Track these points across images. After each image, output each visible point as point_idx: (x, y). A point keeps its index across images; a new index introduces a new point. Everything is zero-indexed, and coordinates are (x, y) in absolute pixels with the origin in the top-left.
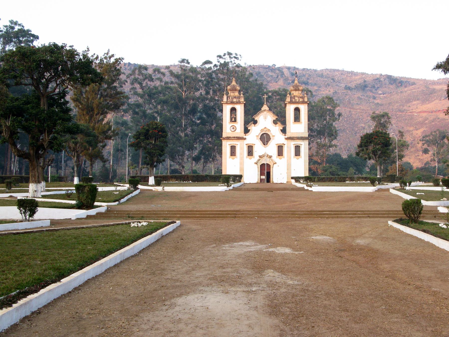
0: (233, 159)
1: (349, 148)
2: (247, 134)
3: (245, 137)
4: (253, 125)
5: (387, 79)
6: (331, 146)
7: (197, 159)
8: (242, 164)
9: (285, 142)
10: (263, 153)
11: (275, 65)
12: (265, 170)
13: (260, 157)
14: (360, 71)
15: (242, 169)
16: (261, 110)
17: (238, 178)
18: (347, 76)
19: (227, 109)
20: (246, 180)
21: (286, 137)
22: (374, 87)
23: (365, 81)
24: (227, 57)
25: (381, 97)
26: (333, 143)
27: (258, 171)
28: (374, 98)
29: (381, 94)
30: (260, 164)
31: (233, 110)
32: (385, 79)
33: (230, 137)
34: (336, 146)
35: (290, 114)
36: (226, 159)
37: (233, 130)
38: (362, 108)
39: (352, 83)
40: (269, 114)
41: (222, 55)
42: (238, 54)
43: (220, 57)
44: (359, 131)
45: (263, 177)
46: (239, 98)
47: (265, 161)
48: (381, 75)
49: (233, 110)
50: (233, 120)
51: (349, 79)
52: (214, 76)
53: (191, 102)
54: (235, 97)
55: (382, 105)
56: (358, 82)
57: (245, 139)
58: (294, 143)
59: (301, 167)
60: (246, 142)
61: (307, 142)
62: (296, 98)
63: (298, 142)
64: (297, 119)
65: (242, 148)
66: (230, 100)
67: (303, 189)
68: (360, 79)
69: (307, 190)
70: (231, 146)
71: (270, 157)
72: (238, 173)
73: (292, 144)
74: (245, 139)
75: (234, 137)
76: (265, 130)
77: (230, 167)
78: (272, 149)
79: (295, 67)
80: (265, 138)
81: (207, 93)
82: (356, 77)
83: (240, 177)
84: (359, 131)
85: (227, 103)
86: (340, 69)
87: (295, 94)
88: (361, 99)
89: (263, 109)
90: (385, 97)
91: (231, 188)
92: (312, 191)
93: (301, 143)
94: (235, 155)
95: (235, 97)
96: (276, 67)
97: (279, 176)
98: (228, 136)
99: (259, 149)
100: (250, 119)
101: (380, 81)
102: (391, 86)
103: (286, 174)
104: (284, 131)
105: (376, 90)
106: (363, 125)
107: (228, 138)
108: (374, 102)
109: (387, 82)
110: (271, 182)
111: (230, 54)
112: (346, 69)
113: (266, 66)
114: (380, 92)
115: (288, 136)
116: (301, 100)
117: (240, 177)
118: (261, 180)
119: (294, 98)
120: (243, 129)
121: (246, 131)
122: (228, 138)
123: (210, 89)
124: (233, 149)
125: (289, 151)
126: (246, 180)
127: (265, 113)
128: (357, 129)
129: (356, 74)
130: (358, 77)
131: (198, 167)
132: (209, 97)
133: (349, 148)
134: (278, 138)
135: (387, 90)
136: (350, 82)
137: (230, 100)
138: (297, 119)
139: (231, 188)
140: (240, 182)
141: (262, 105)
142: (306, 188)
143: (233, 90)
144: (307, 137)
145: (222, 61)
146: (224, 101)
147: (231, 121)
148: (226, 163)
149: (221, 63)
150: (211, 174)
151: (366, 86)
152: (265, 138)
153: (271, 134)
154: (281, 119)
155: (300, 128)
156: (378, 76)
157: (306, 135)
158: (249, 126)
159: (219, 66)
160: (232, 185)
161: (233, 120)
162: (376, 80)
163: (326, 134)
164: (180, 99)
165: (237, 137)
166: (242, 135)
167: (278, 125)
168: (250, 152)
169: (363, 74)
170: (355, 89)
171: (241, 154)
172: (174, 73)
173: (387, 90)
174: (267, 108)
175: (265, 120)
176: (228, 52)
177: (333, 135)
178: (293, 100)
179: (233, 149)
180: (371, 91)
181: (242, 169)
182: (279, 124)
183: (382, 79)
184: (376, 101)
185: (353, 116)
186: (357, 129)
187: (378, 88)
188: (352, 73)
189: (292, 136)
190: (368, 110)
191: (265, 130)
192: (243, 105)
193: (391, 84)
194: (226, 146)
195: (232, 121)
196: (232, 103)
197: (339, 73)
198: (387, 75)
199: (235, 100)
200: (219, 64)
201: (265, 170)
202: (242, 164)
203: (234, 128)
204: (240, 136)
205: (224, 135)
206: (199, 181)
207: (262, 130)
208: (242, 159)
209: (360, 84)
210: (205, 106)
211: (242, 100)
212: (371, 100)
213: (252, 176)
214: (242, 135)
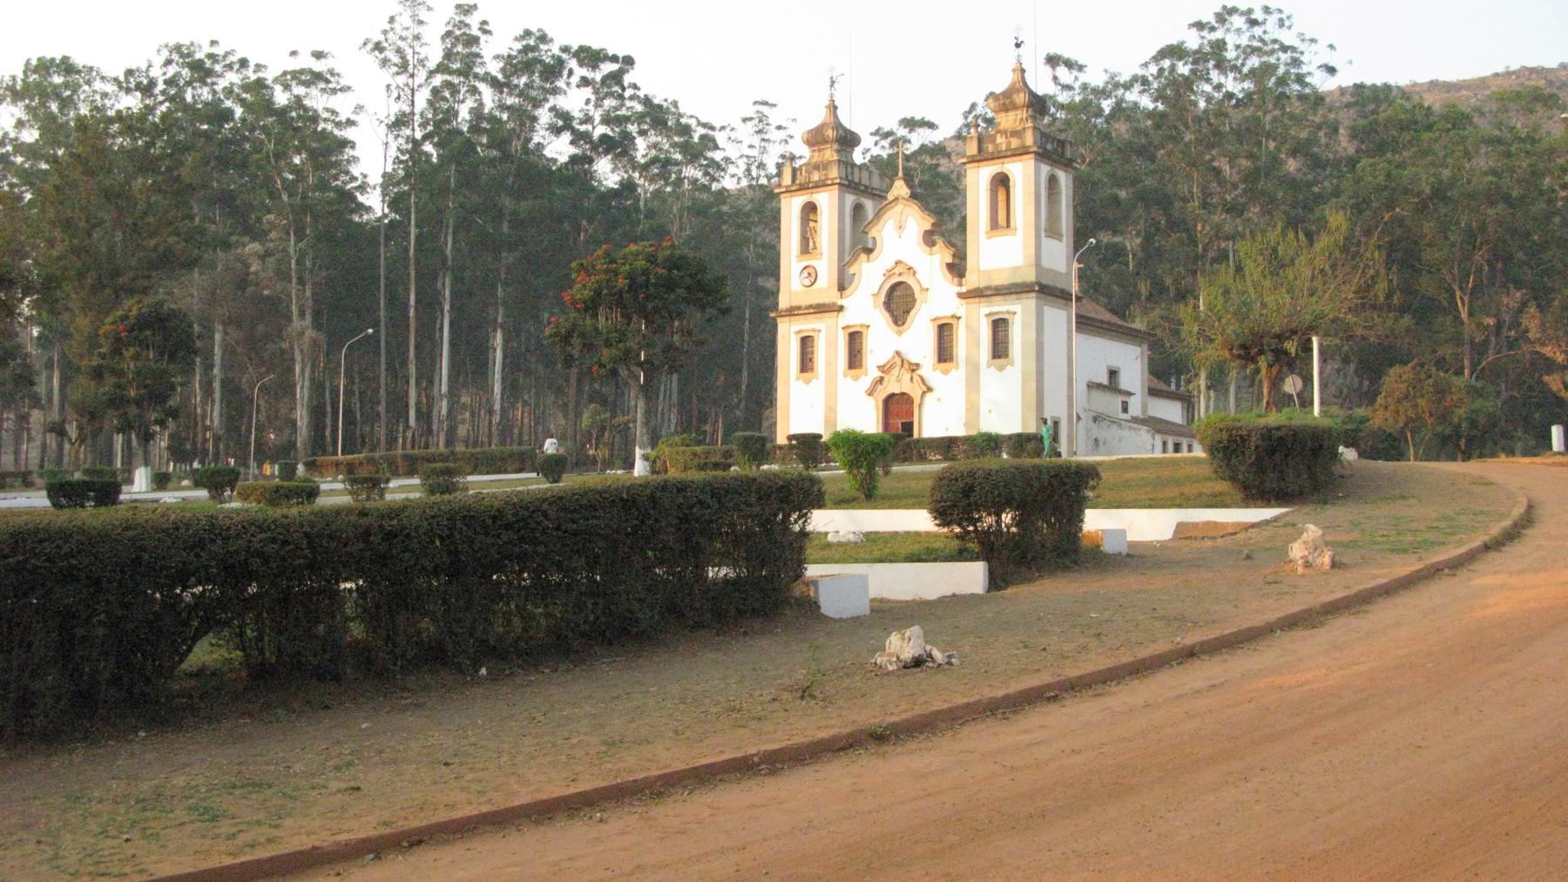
3: (840, 302)
21: (964, 289)
33: (799, 308)
47: (892, 387)
57: (841, 309)
58: (796, 328)
60: (845, 319)
71: (914, 368)
78: (918, 340)
80: (899, 302)
93: (1011, 308)
104: (957, 268)
107: (792, 312)
122: (792, 312)
127: (899, 208)
134: (938, 298)
138: (1000, 221)
152: (899, 302)
154: (947, 226)
191: (896, 271)
194: (788, 337)
196: (803, 188)
203: (811, 274)
205: (784, 302)
207: (889, 274)
214: (832, 296)
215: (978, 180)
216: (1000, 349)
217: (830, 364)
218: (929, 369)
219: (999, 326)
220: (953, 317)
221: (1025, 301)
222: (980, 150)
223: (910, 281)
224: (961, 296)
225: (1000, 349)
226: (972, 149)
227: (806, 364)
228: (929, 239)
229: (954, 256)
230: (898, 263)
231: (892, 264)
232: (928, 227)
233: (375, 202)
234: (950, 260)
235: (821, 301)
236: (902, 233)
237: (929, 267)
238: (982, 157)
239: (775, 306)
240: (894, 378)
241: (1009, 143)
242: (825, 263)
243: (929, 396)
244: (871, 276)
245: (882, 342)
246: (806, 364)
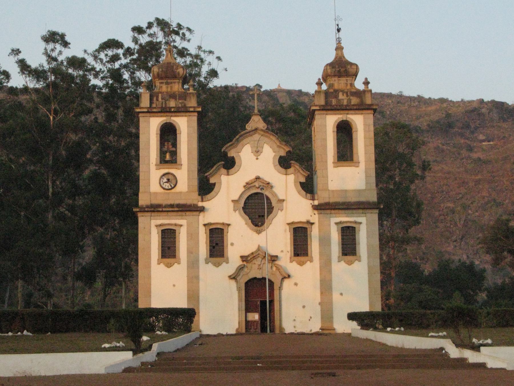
0: (169, 266)
1: (424, 253)
2: (209, 196)
3: (200, 204)
4: (223, 171)
5: (495, 111)
6: (406, 241)
7: (87, 276)
8: (193, 279)
9: (315, 218)
10: (254, 249)
11: (261, 87)
12: (259, 295)
13: (244, 258)
14: (436, 96)
15: (193, 294)
16: (245, 129)
17: (181, 319)
18: (410, 106)
19: (151, 128)
20: (207, 324)
21: (316, 203)
22: (468, 127)
23: (448, 115)
24: (155, 29)
25: (484, 147)
26: (413, 231)
27: (240, 300)
28: (470, 149)
29: (484, 141)
30: (243, 279)
31: (168, 133)
32: (490, 110)
33: (159, 206)
34: (419, 241)
35: (325, 140)
36: (148, 266)
37: (167, 186)
38: (446, 168)
39: (421, 120)
40: (266, 139)
41: (144, 25)
42: (184, 24)
43: (138, 30)
44: (442, 217)
45: (255, 317)
46: (184, 96)
47: (254, 272)
48: (481, 101)
49: (168, 133)
50: (168, 157)
51: (414, 111)
52: (126, 76)
53: (73, 137)
54: (173, 96)
55: (487, 162)
56: (435, 117)
57: (202, 210)
58: (338, 220)
59: (356, 286)
60: (204, 219)
61: (374, 216)
62: (341, 96)
63: (346, 218)
64: (345, 153)
65: (193, 237)
66: (159, 103)
67: (438, 358)
68: (437, 111)
69: (461, 363)
70: (163, 231)
71: (274, 259)
72: (180, 302)
73: (336, 220)
74: (202, 210)
75: (172, 206)
76: (257, 184)
77: (162, 286)
78: (276, 237)
79: (300, 91)
80: (257, 207)
81: (111, 117)
82: (429, 109)
83: (189, 314)
84: (442, 217)
85: (150, 112)
86: (395, 92)
87: (336, 87)
88: (443, 151)
89: (249, 126)
90: (492, 147)
91: (149, 356)
92: (482, 366)
93: (359, 219)
94: (174, 256)
95: (173, 96)
96: (262, 90)
97: (298, 311)
98: (155, 202)
99: (242, 239)
100: (215, 157)
101: (479, 114)
102: (505, 125)
103: (319, 308)
104: (308, 187)
105: (472, 133)
106: (451, 205)
107: (155, 209)
108: (469, 157)
109: (495, 115)
110: (277, 331)
111: (162, 24)
112: (407, 93)
113: (243, 87)
114: (481, 137)
115: (322, 201)
116: (355, 101)
117: (189, 314)
118: (248, 324)
119: (336, 97)
120: (195, 183)
121: (206, 188)
122: (155, 209)
123: (118, 108)
124: (168, 238)
125: (325, 241)
126: (207, 324)
127: (256, 137)
128: (437, 214)
129: (429, 102)
130: (433, 108)
131: (90, 297)
132: (114, 125)
133: (424, 253)
134: (294, 206)
135: (496, 132)
136: (417, 119)
137: (159, 103)
138: (345, 153)
139: (149, 356)
140: (188, 330)
141: (247, 119)
142: (454, 352)
143: (166, 77)
144: (374, 203)
145: (144, 39)
146: (142, 105)
147: (163, 161)
148: (149, 277)
149: (141, 45)
150: (118, 309)
151: (450, 126)
152: (257, 207)
153: (275, 195)
154: (298, 157)
155: (352, 179)
156: (475, 105)
157: (373, 197)
158: (212, 175)
159: (138, 52)
160: (156, 347)
161: (168, 157)
162: (473, 111)
163: (394, 213)
164: (42, 126)
165: (178, 206)
166: (194, 199)
167: (291, 170)
168: (217, 238)
169: (442, 101)
170: (428, 131)
171: (190, 252)
172: (29, 67)
173: (496, 132)
174: (262, 125)
175: (257, 160)
176: (157, 19)
177: (411, 214)
178: (334, 102)
179: (168, 238)
180: (462, 135)
181: (193, 294)
182: (296, 166)
183: (484, 110)
184: (475, 156)
185: (429, 186)
186: (437, 214)
187: (476, 128)
188: (420, 99)
189: (332, 200)
190: (459, 173)
191: (257, 184)
192: (194, 118)
193: (504, 120)
194: (149, 234)
195: (167, 162)
196: (165, 111)
197: (394, 100)
198: (493, 102)
199: (172, 104)
200: (137, 47)
201: (259, 295)
202: (193, 279)
203: (171, 180)
204: (189, 202)
205: (143, 200)
206: (60, 331)
207: (248, 185)
208: (193, 265)
209: (438, 122)
210: (105, 147)
211: (192, 103)
212: (464, 153)
213: (221, 313)
214: (194, 199)
215: (327, 125)
216: (349, 247)
217: (192, 252)
218: (286, 261)
219: (348, 235)
220: (308, 222)
221: (368, 215)
222: (326, 102)
223: (266, 193)
224: (316, 208)
225: (349, 247)
226: (322, 102)
227: (168, 249)
228: (284, 163)
229: (313, 94)
230: (258, 178)
231: (253, 177)
232: (283, 153)
233: (90, 85)
234: (303, 180)
235: (182, 202)
236: (257, 160)
237: (285, 185)
238: (328, 108)
239: (137, 205)
240: (256, 266)
241: (349, 101)
242: (185, 174)
243: (286, 283)
244: (230, 186)
245: (242, 239)
246: (168, 249)
